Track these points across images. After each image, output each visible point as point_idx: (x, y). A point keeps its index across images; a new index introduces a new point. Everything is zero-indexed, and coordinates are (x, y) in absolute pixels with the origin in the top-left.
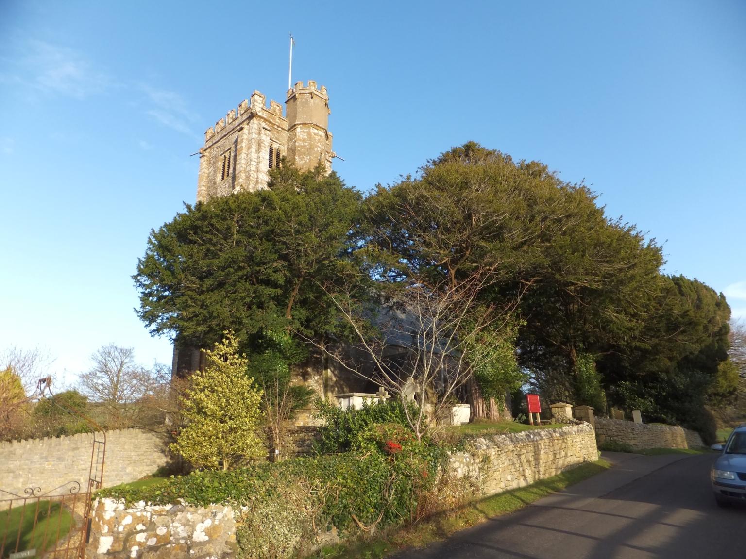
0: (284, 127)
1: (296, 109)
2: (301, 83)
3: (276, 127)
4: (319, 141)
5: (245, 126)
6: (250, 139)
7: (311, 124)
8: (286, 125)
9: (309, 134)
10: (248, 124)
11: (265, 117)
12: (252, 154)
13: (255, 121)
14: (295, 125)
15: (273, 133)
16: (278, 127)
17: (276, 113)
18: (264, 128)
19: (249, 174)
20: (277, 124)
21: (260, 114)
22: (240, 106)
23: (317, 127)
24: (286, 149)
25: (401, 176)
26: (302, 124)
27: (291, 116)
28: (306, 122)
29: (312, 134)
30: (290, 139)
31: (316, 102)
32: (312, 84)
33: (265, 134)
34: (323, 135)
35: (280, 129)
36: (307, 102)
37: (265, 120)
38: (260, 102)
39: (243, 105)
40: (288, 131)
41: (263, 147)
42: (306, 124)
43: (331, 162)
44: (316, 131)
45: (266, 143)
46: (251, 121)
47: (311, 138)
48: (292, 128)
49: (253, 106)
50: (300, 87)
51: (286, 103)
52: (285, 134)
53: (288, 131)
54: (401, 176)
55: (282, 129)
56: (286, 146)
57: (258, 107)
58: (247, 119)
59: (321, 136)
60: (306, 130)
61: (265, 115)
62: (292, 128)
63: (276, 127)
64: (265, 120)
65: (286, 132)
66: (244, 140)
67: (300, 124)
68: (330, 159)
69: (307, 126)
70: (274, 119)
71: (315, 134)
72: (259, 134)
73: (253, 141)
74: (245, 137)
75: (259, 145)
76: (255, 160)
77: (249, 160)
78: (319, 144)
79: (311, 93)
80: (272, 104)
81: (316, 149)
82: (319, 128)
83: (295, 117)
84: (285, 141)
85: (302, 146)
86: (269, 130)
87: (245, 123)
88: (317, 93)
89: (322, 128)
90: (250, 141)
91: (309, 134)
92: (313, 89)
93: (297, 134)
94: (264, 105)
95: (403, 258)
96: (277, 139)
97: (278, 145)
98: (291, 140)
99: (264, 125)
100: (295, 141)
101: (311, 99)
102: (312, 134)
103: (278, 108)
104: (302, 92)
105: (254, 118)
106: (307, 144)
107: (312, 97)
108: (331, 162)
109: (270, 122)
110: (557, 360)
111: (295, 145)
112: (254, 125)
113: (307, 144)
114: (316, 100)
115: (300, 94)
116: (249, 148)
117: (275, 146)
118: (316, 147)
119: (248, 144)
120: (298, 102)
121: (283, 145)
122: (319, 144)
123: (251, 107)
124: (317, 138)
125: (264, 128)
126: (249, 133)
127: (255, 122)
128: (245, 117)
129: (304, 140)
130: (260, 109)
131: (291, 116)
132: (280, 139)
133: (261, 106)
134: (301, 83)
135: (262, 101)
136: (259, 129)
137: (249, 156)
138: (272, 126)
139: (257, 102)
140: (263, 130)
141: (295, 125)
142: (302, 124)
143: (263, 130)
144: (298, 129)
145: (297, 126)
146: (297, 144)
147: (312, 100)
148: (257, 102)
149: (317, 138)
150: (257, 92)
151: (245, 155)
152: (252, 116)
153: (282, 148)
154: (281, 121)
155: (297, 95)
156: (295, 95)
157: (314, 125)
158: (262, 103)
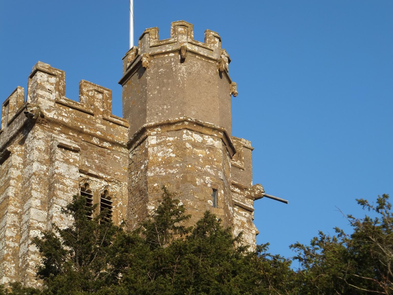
0: (117, 139)
1: (145, 93)
2: (152, 31)
3: (95, 141)
4: (207, 160)
5: (16, 148)
6: (27, 176)
7: (183, 121)
8: (123, 135)
9: (179, 146)
10: (22, 142)
11: (66, 120)
12: (33, 211)
13: (39, 134)
14: (144, 130)
15: (89, 157)
16: (102, 139)
17: (96, 109)
18: (61, 146)
19: (24, 262)
20: (99, 133)
21: (50, 115)
22: (7, 104)
23: (199, 129)
24: (125, 190)
25: (362, 203)
26: (161, 125)
27: (135, 110)
28: (171, 119)
29: (188, 145)
30: (134, 166)
31: (194, 69)
32: (180, 29)
33: (67, 161)
34: (218, 144)
35: (106, 144)
36: (170, 73)
37: (66, 128)
38: (52, 88)
39: (12, 102)
40: (129, 146)
41: (59, 193)
42: (169, 124)
43: (250, 211)
44: (197, 138)
45: (68, 182)
46: (30, 135)
47: (184, 155)
48: (137, 137)
49: (33, 98)
50: (151, 40)
51: (122, 82)
52: (122, 156)
53: (129, 146)
54: (362, 203)
55: (114, 143)
56: (125, 184)
57: (46, 96)
58: (20, 130)
59: (211, 148)
60: (171, 139)
61: (66, 116)
62: (138, 139)
63: (95, 141)
64: (66, 128)
65: (124, 150)
66: (12, 182)
67: (156, 126)
68: (249, 204)
69: (173, 127)
70: (91, 124)
71: (195, 145)
72: (51, 161)
73: (34, 180)
74: (15, 173)
75: (51, 188)
76: (41, 225)
77: (25, 227)
78: (207, 168)
79: (179, 51)
80: (85, 90)
81: (199, 181)
82: (204, 130)
83: (144, 111)
84: (121, 171)
85: (163, 178)
86: (76, 151)
87: (17, 140)
88: (196, 49)
89: (214, 129)
90: (26, 181)
91: (179, 146)
92: (184, 40)
93: (150, 150)
94: (62, 93)
95: (155, 184)
96: (99, 168)
97: (106, 183)
98: (137, 168)
99: (63, 139)
100: (146, 169)
101: (180, 65)
102: (188, 145)
103: (100, 96)
104: (158, 50)
105: (37, 126)
106: (175, 171)
107: (183, 60)
108: (250, 211)
109: (80, 132)
110: (49, 111)
111: (146, 177)
112: (36, 143)
113: (175, 171)
114: (195, 65)
115: (152, 56)
116: (25, 197)
117: (96, 186)
118: (200, 176)
119: (24, 188)
120: (148, 76)
121: (118, 182)
122: (207, 168)
123: (29, 101)
124: (201, 153)
125: (61, 146)
126: (25, 164)
127: (38, 137)
128: (16, 127)
129: (168, 163)
130: (52, 104)
131: (135, 110)
132: (109, 168)
133: (53, 96)
134: (152, 31)
135: (57, 84)
136: (50, 151)
137: (25, 218)
138: (84, 140)
139: (43, 88)
140: (59, 153)
141: (144, 130)
142: (161, 125)
143: (59, 151)
144: (152, 140)
145: (149, 131)
146: (149, 174)
147: (183, 67)
148: (43, 88)
149: (201, 153)
150: (40, 65)
151: (16, 218)
152: (31, 121)
153: (114, 189)
154: (109, 127)
155: (145, 60)
156: (140, 62)
157: (191, 123)
158: (57, 89)
